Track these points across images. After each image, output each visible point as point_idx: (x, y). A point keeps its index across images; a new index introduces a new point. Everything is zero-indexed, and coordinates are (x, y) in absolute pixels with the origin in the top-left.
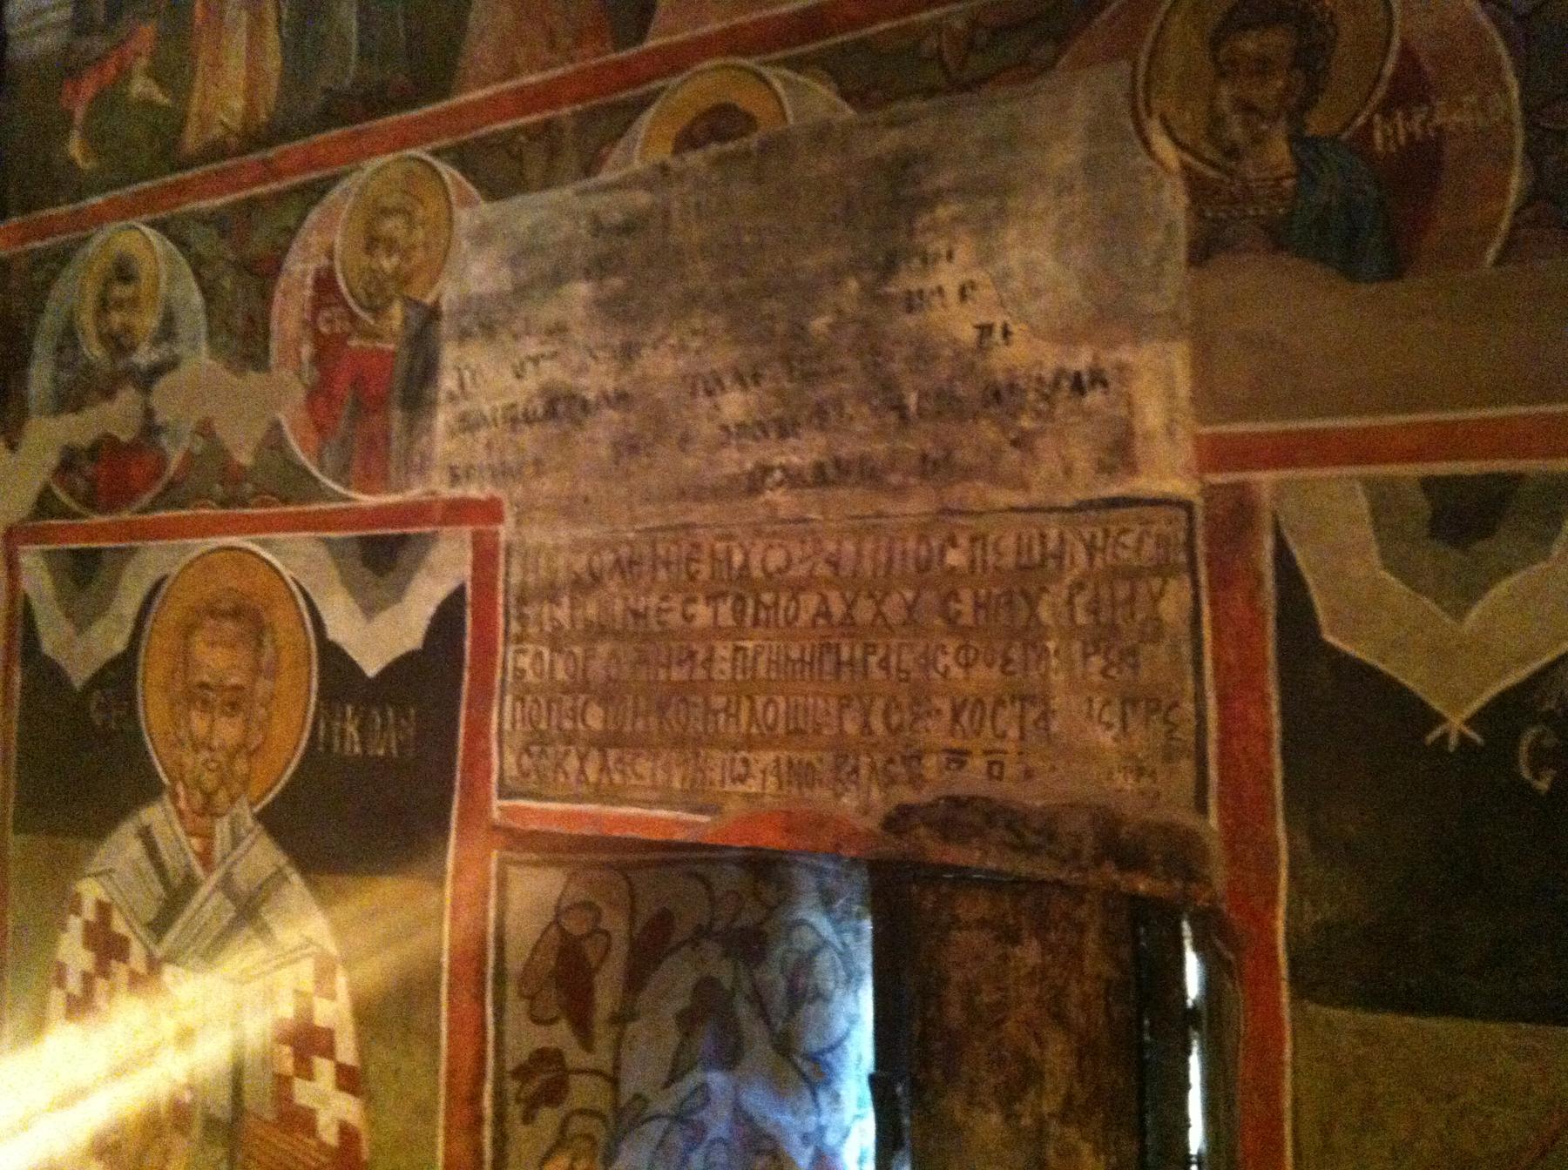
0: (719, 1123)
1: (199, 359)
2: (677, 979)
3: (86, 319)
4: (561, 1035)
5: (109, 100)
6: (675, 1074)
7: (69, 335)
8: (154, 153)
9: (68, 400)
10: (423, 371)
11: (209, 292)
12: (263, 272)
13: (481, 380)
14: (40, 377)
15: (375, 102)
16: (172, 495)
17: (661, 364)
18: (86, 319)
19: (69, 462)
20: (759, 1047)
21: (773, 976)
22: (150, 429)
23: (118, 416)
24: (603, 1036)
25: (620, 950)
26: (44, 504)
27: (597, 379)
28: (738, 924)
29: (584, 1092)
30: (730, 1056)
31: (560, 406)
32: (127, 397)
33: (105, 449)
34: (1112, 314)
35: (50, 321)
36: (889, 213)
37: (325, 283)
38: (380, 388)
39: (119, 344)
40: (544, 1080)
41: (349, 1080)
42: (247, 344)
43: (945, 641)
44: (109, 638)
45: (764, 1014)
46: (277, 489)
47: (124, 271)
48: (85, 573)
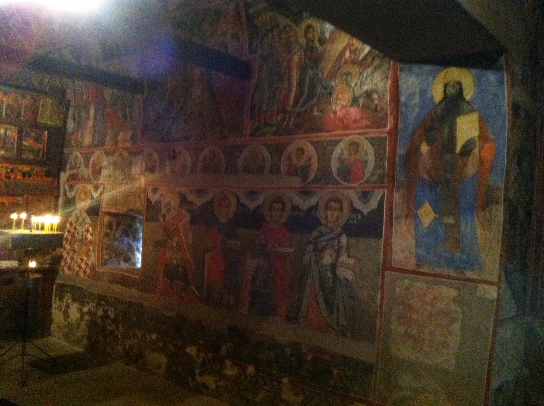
0: (126, 242)
1: (83, 167)
2: (122, 227)
3: (73, 161)
4: (109, 231)
5: (76, 139)
6: (121, 236)
7: (71, 162)
8: (79, 145)
9: (70, 169)
10: (101, 171)
11: (84, 161)
12: (89, 160)
13: (105, 172)
14: (68, 166)
15: (98, 146)
16: (80, 180)
17: (117, 173)
18: (73, 161)
19: (70, 175)
20: (131, 235)
21: (133, 229)
22: (78, 174)
23: (75, 171)
24: (113, 232)
25: (115, 224)
26: (68, 180)
27: (112, 174)
28: (494, 385)
29: (111, 236)
30: (127, 236)
31: (110, 176)
32: (76, 170)
33: (74, 174)
34: (141, 174)
35: (69, 161)
36: (130, 164)
37: (94, 162)
38: (97, 172)
39: (76, 164)
40: (107, 235)
41: (91, 234)
42: (87, 166)
43: (205, 199)
44: (73, 194)
45: (132, 232)
46: (88, 181)
47: (77, 157)
48: (71, 187)
